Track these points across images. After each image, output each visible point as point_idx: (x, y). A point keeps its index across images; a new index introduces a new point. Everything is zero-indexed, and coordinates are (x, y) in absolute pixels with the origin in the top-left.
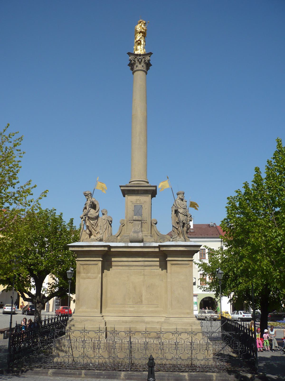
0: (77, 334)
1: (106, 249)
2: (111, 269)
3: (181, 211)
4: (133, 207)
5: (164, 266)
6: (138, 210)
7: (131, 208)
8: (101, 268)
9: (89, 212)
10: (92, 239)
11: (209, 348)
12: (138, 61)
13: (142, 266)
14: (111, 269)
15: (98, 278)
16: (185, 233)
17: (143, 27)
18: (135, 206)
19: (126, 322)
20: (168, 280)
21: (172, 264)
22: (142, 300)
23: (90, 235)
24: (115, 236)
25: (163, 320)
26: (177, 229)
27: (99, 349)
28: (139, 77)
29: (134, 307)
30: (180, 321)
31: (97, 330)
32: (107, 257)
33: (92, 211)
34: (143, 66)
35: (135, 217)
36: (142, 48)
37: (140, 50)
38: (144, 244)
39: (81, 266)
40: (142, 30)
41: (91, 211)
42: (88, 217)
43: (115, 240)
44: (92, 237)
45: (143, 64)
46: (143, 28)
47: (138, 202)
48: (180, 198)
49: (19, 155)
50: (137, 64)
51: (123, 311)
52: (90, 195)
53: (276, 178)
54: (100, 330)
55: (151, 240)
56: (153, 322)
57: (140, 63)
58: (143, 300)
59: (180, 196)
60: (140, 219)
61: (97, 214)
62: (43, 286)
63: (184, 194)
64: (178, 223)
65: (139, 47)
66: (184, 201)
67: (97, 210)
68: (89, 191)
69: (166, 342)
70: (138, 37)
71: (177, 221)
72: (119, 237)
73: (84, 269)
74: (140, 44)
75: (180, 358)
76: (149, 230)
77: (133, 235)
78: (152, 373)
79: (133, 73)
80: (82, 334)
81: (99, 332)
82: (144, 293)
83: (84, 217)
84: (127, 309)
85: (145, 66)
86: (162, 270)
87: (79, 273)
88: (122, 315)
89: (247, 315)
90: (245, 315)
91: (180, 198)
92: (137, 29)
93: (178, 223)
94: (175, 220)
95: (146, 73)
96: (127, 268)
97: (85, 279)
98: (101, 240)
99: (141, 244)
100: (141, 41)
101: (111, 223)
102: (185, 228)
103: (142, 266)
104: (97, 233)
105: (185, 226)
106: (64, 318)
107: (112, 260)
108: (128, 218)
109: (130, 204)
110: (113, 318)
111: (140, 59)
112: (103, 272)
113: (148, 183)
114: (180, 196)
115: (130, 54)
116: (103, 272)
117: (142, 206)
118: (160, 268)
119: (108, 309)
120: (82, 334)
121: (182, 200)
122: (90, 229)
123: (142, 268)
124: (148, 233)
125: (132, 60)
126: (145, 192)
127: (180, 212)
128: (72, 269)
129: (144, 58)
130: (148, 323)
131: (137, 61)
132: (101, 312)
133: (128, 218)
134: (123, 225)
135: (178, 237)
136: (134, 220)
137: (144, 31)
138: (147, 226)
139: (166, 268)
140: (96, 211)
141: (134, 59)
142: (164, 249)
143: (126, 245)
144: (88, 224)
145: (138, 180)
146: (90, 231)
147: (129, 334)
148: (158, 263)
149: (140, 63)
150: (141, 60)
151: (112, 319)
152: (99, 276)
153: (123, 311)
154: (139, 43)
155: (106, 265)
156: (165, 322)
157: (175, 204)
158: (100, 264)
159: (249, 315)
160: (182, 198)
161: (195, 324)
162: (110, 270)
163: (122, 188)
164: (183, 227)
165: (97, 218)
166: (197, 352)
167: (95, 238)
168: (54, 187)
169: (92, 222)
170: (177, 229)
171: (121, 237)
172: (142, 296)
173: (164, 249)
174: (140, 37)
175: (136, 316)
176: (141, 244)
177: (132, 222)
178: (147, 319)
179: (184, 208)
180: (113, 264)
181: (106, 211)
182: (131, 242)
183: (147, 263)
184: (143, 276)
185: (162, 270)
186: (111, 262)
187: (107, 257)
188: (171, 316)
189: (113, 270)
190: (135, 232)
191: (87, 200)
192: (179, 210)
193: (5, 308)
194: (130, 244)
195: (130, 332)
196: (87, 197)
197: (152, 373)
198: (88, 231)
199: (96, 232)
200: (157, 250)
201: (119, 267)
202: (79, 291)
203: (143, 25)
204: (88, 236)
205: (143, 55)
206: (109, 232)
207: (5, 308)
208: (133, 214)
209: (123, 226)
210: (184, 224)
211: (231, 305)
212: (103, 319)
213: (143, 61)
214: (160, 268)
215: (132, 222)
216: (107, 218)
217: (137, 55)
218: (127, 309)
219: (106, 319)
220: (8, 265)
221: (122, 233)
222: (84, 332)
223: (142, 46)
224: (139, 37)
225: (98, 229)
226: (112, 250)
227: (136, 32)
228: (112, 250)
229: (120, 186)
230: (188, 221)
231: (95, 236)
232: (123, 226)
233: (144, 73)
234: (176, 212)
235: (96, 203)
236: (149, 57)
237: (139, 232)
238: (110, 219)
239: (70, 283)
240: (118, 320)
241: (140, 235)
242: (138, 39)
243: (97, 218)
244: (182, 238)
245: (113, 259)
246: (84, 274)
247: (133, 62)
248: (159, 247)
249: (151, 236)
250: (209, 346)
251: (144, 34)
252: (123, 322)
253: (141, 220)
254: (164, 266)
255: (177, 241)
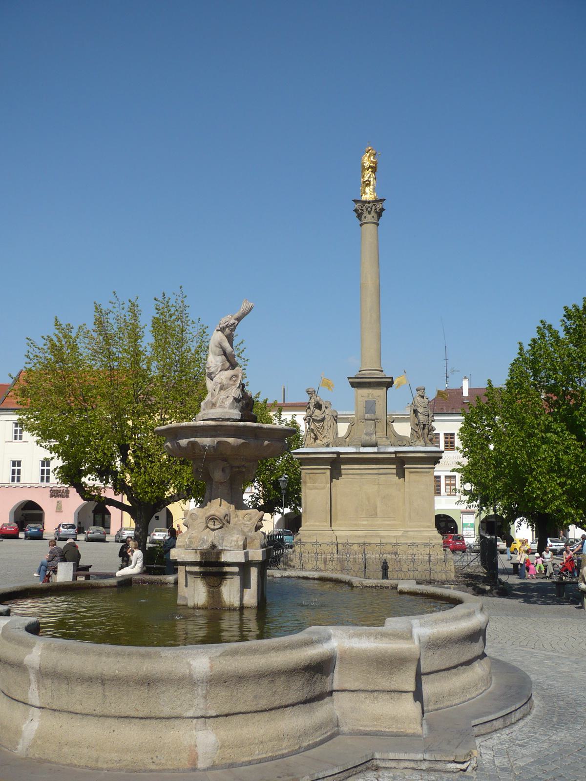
0: (308, 547)
1: (335, 456)
2: (340, 478)
3: (420, 410)
4: (365, 402)
5: (401, 474)
6: (370, 407)
7: (362, 404)
8: (329, 477)
9: (313, 413)
10: (317, 445)
12: (367, 209)
13: (376, 474)
14: (340, 478)
15: (327, 488)
16: (426, 435)
17: (372, 160)
18: (366, 401)
19: (359, 537)
20: (406, 490)
21: (187, 573)
22: (376, 513)
23: (316, 439)
24: (343, 437)
25: (400, 534)
26: (416, 432)
27: (332, 562)
28: (369, 229)
29: (368, 521)
30: (419, 534)
32: (336, 465)
33: (317, 412)
34: (373, 217)
35: (367, 416)
36: (371, 190)
37: (369, 195)
38: (378, 449)
40: (372, 165)
41: (315, 411)
42: (313, 419)
43: (343, 442)
44: (318, 441)
45: (373, 213)
46: (372, 161)
47: (370, 397)
48: (420, 395)
49: (244, 363)
50: (366, 214)
51: (356, 525)
52: (313, 393)
54: (332, 543)
55: (387, 443)
56: (389, 536)
57: (369, 213)
58: (378, 512)
59: (420, 393)
60: (373, 418)
61: (323, 416)
62: (244, 498)
63: (424, 390)
64: (417, 425)
65: (367, 190)
66: (425, 397)
67: (323, 411)
68: (312, 388)
69: (402, 557)
70: (366, 175)
71: (416, 422)
72: (348, 438)
73: (310, 478)
74: (368, 185)
75: (417, 570)
76: (384, 431)
77: (366, 439)
78: (385, 575)
79: (361, 225)
82: (379, 504)
83: (307, 418)
84: (360, 522)
85: (376, 216)
86: (399, 478)
87: (305, 482)
89: (557, 544)
90: (553, 544)
91: (420, 395)
92: (364, 165)
93: (417, 425)
94: (414, 422)
95: (378, 225)
96: (359, 476)
97: (311, 489)
98: (328, 446)
99: (375, 450)
100: (370, 181)
101: (336, 418)
102: (426, 431)
103: (376, 474)
104: (324, 437)
105: (426, 427)
106: (280, 537)
107: (342, 468)
108: (358, 416)
110: (343, 532)
111: (369, 207)
112: (331, 481)
113: (382, 371)
114: (420, 393)
115: (356, 201)
116: (331, 481)
117: (375, 401)
118: (397, 476)
119: (338, 522)
121: (423, 397)
122: (315, 432)
124: (383, 435)
125: (358, 209)
126: (379, 385)
127: (419, 411)
128: (287, 476)
129: (374, 205)
130: (382, 537)
131: (365, 210)
132: (331, 526)
133: (358, 416)
134: (352, 424)
135: (418, 442)
136: (366, 420)
137: (374, 165)
138: (381, 426)
139: (404, 477)
140: (321, 412)
141: (362, 207)
142: (401, 455)
143: (358, 451)
144: (312, 427)
145: (370, 369)
146: (315, 435)
147: (363, 547)
148: (394, 471)
149: (369, 213)
150: (371, 209)
151: (343, 534)
152: (327, 486)
153: (356, 525)
154: (367, 184)
155: (335, 474)
156: (402, 536)
157: (413, 403)
158: (328, 472)
159: (560, 544)
160: (422, 395)
161: (435, 538)
162: (339, 479)
163: (351, 380)
164: (424, 429)
165: (323, 420)
166: (423, 552)
167: (322, 443)
169: (317, 424)
170: (416, 432)
171: (350, 439)
172: (376, 508)
173: (401, 455)
174: (368, 176)
175: (371, 530)
176: (375, 450)
177: (363, 421)
178: (382, 533)
179: (424, 406)
180: (343, 472)
181: (330, 404)
182: (364, 446)
184: (377, 486)
185: (399, 478)
186: (341, 469)
187: (336, 465)
188: (410, 530)
189: (343, 478)
190: (367, 434)
191: (311, 399)
192: (419, 410)
193: (155, 535)
194: (363, 450)
195: (364, 544)
196: (310, 395)
197: (385, 575)
198: (312, 435)
199: (323, 436)
200: (393, 456)
201: (350, 476)
202: (305, 502)
203: (372, 157)
204: (312, 440)
205: (373, 202)
206: (334, 431)
207: (155, 535)
208: (365, 412)
209: (352, 425)
210: (424, 425)
211: (533, 531)
212: (334, 533)
213: (373, 210)
214: (397, 476)
215: (363, 421)
216: (331, 412)
217: (366, 202)
218: (360, 522)
219: (337, 533)
220: (179, 469)
221: (352, 434)
223: (371, 187)
224: (368, 175)
225: (324, 433)
226: (342, 456)
227: (364, 169)
228: (342, 456)
229: (349, 378)
230: (430, 421)
231: (321, 440)
232: (352, 425)
233: (376, 226)
234: (415, 412)
235: (321, 402)
236: (380, 204)
237: (372, 434)
238: (335, 414)
239: (284, 494)
240: (350, 534)
241: (374, 438)
242: (366, 179)
243: (323, 420)
244: (422, 442)
245: (343, 467)
246: (311, 483)
247: (360, 211)
248: (396, 453)
249: (386, 438)
251: (374, 169)
252: (356, 536)
253: (374, 419)
254: (401, 474)
255: (416, 446)
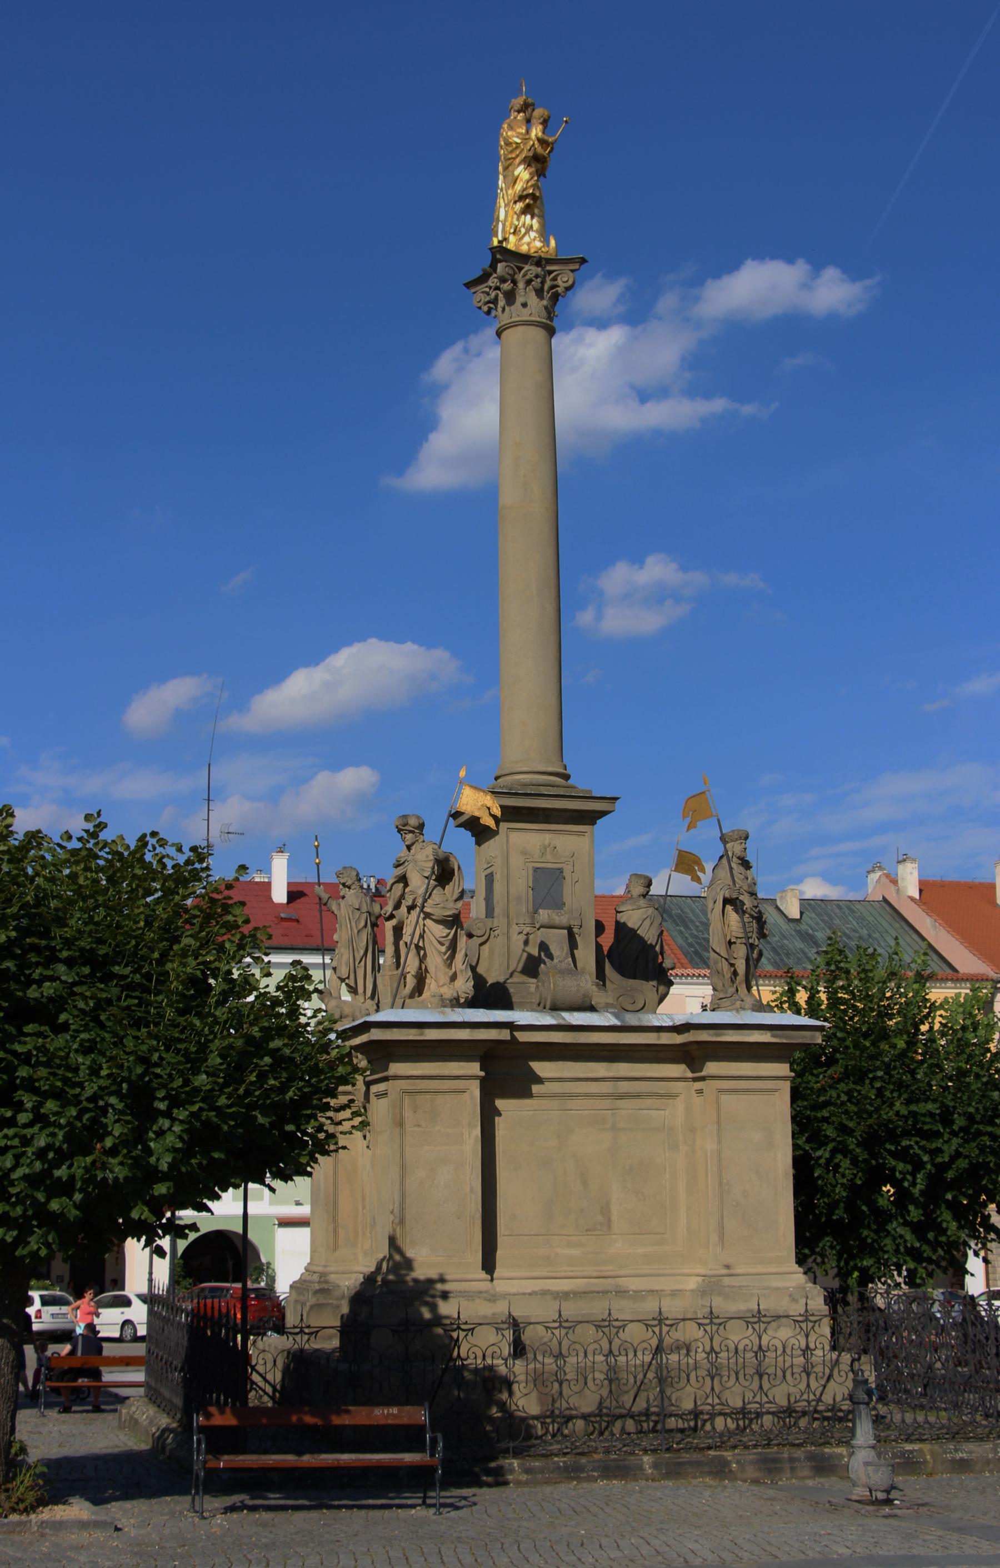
4: (531, 872)
11: (813, 1367)
31: (554, 1321)
39: (407, 1100)
47: (548, 857)
53: (207, 1029)
58: (614, 1217)
80: (654, 1332)
81: (560, 1326)
88: (545, 1274)
109: (516, 861)
120: (654, 1332)
123: (607, 1103)
147: (657, 1329)
168: (271, 767)
178: (633, 1284)
183: (624, 1087)
195: (660, 1321)
222: (560, 1326)
250: (514, 1369)
